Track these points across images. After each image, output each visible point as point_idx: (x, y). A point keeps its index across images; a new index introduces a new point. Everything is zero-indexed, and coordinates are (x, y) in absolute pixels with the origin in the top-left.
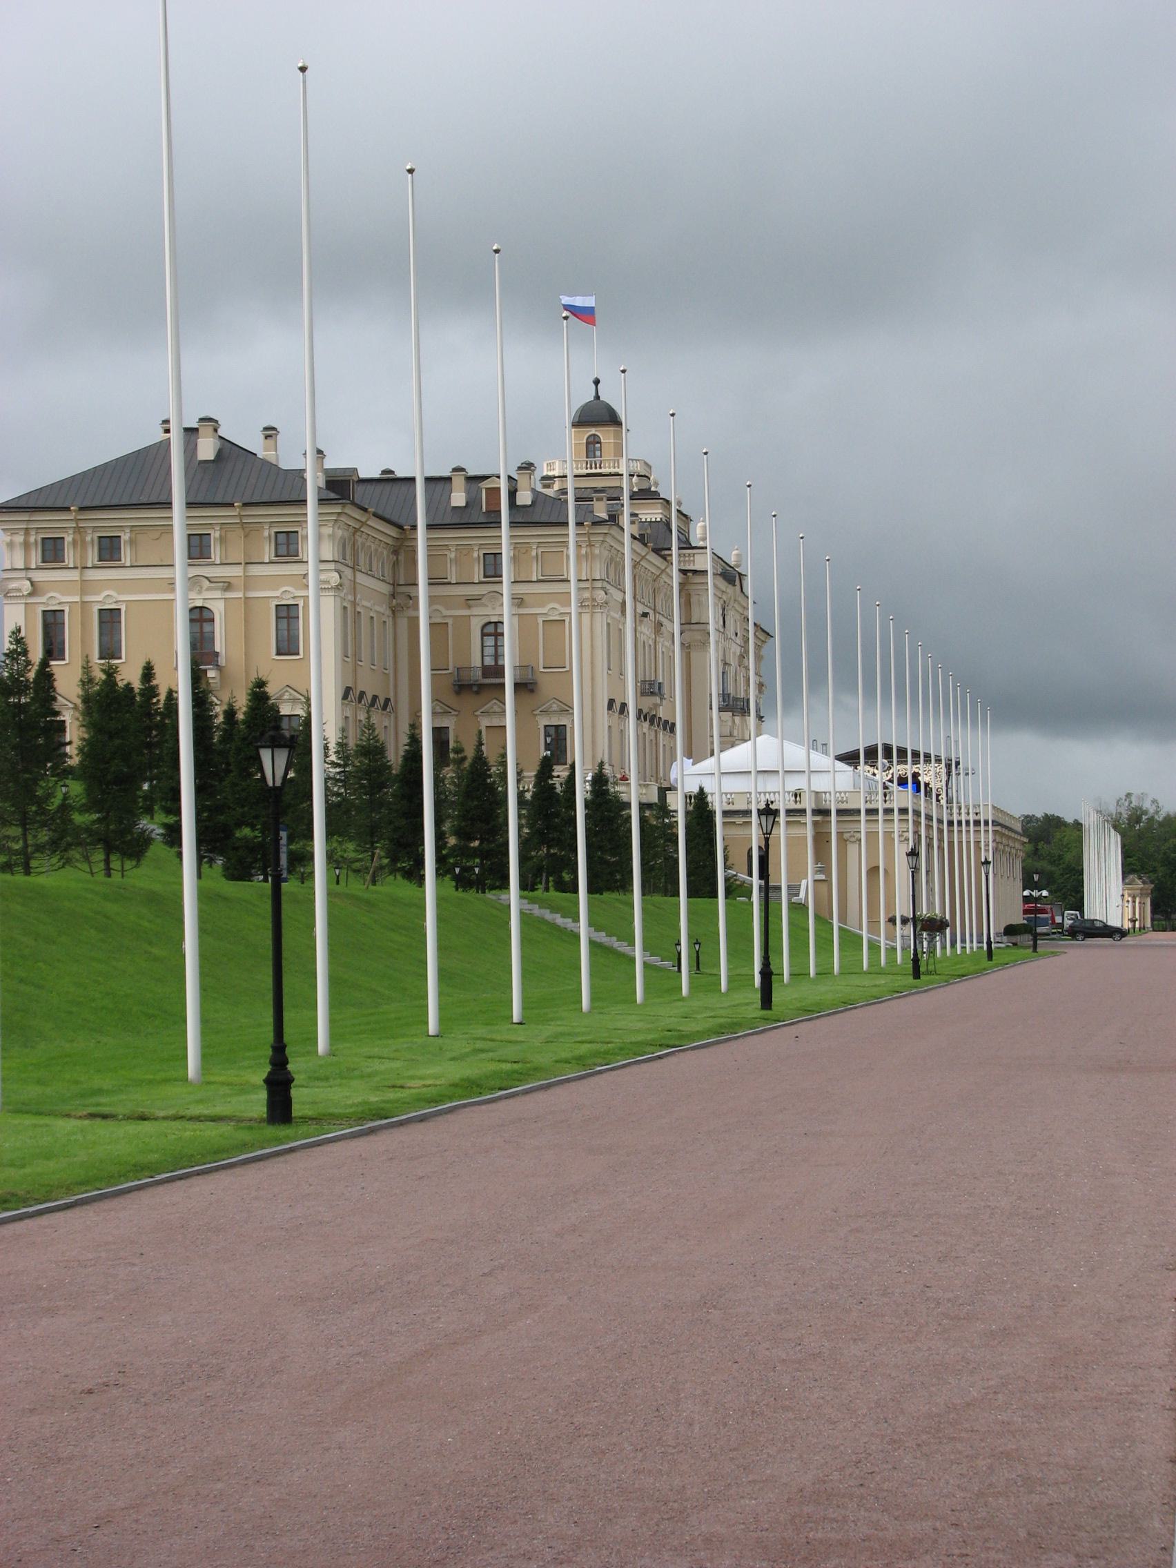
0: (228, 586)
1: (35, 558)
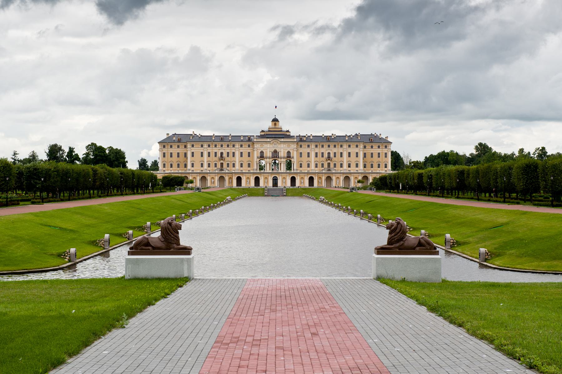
0: (332, 150)
1: (162, 147)
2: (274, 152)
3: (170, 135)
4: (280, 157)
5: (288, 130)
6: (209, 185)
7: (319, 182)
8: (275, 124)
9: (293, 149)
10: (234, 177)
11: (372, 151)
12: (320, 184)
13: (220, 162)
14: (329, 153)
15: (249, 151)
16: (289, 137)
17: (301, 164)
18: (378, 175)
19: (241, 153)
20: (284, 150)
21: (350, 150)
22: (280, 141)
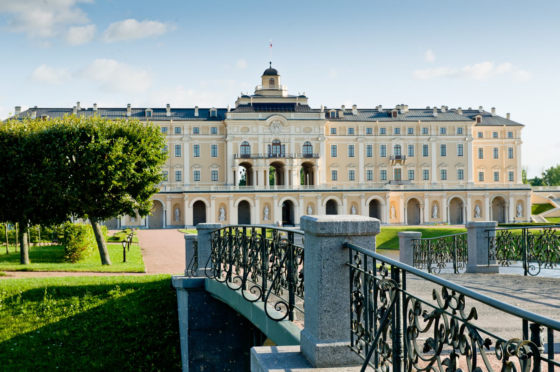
2: (273, 144)
3: (23, 110)
4: (287, 155)
5: (301, 94)
6: (512, 219)
7: (476, 212)
8: (272, 82)
9: (317, 137)
10: (186, 203)
11: (444, 140)
12: (265, 219)
13: (394, 167)
14: (398, 147)
15: (214, 142)
16: (306, 108)
17: (334, 173)
18: (445, 194)
19: (443, 147)
20: (296, 139)
21: (446, 140)
22: (288, 120)
